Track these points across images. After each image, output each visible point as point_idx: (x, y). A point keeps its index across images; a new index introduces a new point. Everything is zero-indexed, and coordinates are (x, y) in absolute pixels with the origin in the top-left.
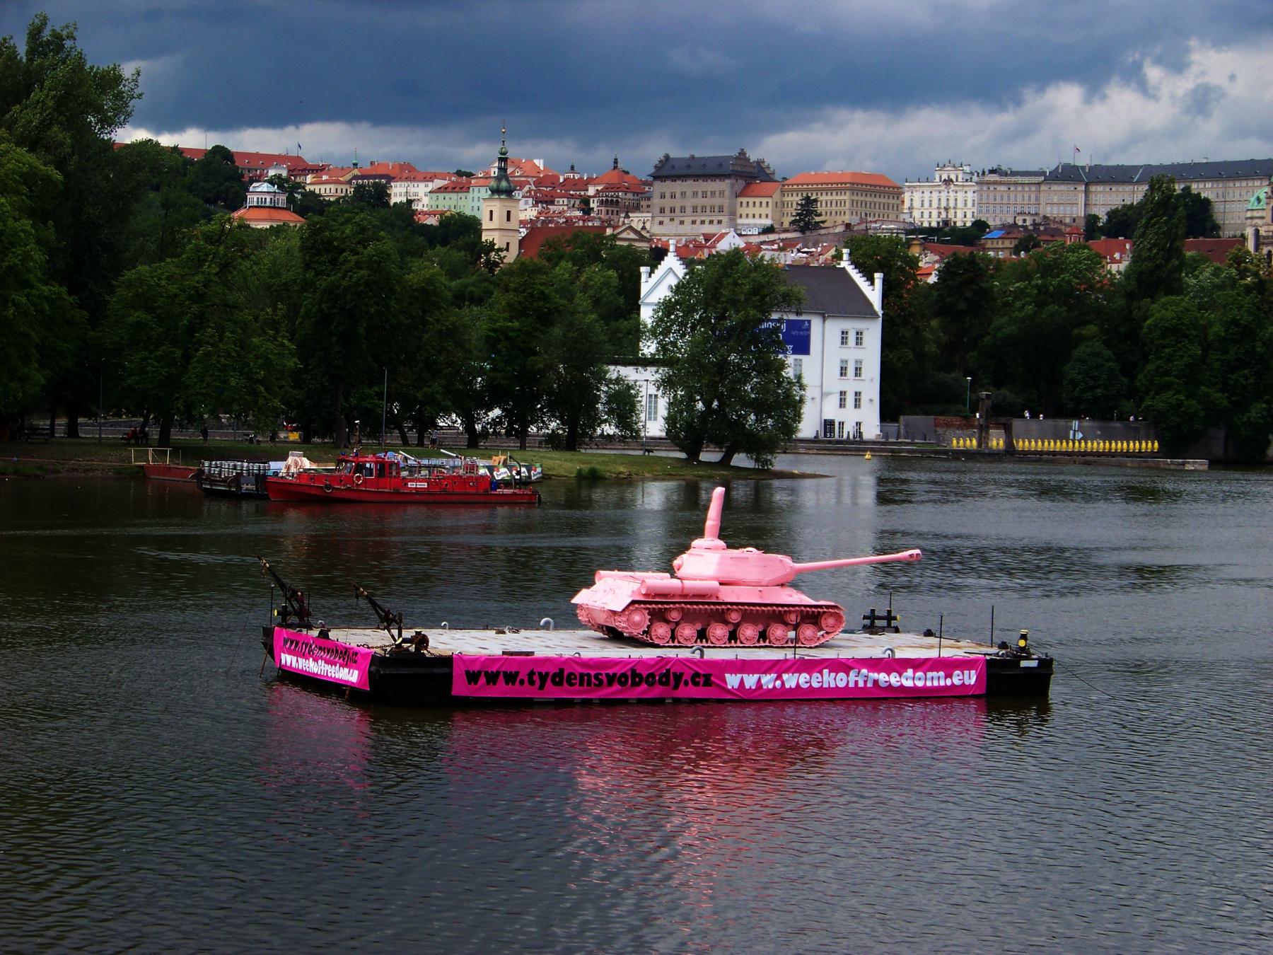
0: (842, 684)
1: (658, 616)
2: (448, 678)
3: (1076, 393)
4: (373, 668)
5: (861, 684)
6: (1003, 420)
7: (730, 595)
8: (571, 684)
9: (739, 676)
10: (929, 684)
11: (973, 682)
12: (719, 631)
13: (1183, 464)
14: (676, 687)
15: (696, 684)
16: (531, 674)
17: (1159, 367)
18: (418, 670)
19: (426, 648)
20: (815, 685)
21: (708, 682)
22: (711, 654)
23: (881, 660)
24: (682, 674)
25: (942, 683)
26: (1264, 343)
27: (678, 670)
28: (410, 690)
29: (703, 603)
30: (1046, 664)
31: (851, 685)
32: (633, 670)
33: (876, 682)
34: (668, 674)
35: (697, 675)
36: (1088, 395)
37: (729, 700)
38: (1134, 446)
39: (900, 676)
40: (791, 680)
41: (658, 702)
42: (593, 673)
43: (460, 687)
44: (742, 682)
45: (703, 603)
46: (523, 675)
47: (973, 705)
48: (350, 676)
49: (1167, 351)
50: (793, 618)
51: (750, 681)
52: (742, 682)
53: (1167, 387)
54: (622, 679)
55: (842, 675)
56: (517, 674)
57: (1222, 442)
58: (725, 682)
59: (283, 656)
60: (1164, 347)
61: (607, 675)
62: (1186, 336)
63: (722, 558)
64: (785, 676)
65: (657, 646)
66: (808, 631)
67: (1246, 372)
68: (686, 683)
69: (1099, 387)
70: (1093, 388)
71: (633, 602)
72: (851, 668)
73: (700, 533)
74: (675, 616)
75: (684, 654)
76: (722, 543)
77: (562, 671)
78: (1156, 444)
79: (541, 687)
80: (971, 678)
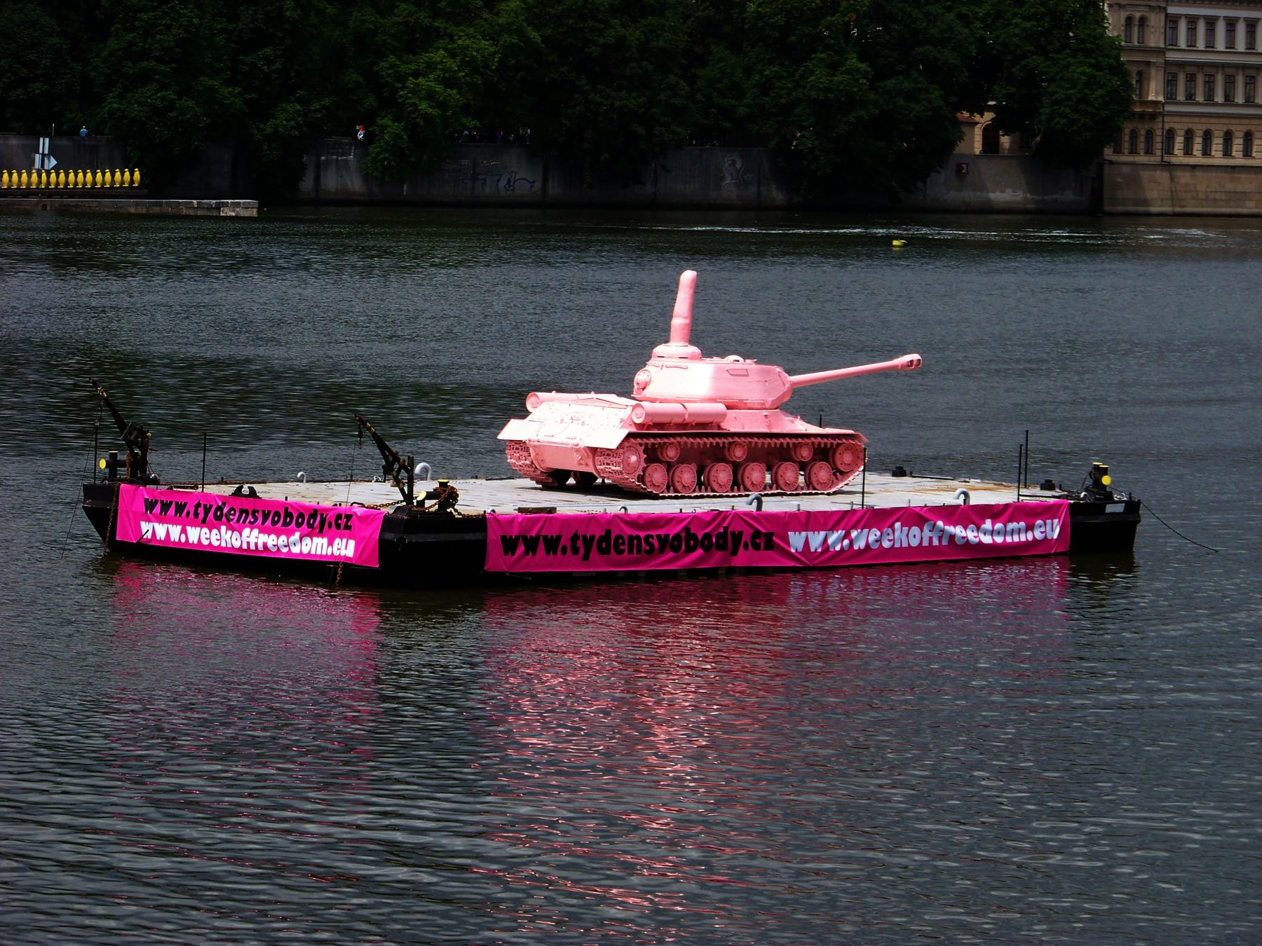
0: (914, 543)
1: (652, 456)
2: (481, 546)
4: (389, 536)
7: (736, 423)
8: (620, 552)
9: (804, 534)
10: (1009, 539)
12: (789, 473)
13: (218, 208)
14: (734, 553)
15: (756, 547)
16: (575, 537)
18: (442, 537)
19: (453, 506)
21: (770, 545)
22: (773, 505)
23: (1007, 506)
24: (741, 533)
25: (1023, 538)
28: (430, 565)
29: (700, 436)
30: (1133, 507)
32: (687, 529)
33: (952, 537)
34: (723, 534)
35: (757, 534)
37: (794, 570)
38: (103, 178)
39: (978, 529)
40: (862, 538)
41: (712, 573)
43: (497, 561)
44: (807, 543)
45: (700, 436)
46: (565, 541)
48: (345, 548)
49: (144, 17)
50: (805, 453)
51: (816, 540)
52: (807, 543)
55: (915, 530)
56: (559, 537)
58: (788, 543)
59: (145, 526)
61: (659, 537)
63: (718, 370)
65: (656, 497)
66: (822, 472)
67: (268, 50)
68: (564, 551)
71: (630, 435)
74: (671, 453)
76: (694, 350)
77: (608, 532)
78: (137, 175)
79: (586, 558)
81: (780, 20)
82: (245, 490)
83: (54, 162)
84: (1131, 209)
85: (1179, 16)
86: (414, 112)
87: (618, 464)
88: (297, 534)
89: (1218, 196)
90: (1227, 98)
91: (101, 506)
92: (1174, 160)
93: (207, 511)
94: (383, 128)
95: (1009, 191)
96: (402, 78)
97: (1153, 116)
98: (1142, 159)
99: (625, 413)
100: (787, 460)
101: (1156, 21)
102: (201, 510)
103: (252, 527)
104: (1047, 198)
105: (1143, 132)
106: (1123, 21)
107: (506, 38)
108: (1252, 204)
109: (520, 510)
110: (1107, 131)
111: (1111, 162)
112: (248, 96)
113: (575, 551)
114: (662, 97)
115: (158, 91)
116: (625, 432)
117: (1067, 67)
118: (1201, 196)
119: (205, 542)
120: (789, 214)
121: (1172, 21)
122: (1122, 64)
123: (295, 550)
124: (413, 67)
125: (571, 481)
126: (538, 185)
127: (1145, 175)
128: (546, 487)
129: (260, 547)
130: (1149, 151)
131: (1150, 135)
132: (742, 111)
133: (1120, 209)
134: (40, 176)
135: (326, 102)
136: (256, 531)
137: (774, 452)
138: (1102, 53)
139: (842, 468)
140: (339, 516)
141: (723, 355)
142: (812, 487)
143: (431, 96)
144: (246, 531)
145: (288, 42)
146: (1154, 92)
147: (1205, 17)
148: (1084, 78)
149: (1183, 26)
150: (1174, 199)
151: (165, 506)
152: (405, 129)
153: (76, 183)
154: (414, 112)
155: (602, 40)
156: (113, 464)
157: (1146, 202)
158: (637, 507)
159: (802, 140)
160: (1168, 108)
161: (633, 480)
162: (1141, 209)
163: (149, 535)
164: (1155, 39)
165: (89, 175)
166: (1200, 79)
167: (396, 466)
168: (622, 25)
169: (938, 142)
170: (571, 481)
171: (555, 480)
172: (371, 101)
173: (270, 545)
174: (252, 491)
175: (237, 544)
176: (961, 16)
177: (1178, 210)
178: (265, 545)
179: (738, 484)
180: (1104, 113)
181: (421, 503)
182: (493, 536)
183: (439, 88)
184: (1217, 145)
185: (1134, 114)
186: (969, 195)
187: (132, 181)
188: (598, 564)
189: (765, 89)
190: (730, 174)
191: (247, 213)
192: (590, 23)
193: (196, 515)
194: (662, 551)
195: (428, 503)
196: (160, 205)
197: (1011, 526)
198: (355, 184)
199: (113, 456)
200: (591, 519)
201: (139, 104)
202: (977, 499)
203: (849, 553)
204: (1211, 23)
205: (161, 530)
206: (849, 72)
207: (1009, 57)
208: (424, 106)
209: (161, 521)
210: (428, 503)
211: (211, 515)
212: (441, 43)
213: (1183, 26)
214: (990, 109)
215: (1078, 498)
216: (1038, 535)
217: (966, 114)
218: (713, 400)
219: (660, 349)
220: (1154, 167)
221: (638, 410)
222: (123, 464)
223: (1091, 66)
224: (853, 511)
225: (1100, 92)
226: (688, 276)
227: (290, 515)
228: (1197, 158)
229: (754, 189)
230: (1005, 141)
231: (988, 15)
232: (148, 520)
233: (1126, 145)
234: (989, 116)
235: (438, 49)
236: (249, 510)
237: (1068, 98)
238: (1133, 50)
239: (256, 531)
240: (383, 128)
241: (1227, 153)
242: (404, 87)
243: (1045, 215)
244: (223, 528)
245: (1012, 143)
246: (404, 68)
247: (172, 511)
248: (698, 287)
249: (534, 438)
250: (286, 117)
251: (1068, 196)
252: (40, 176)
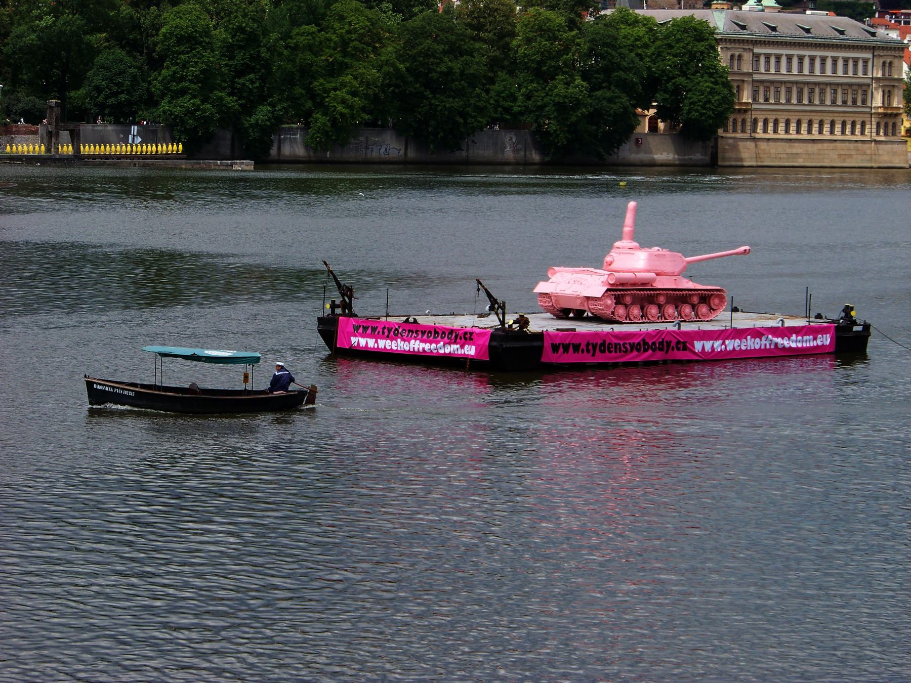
0: (757, 347)
1: (619, 300)
2: (541, 348)
3: (100, 99)
4: (494, 344)
5: (768, 347)
6: (71, 127)
7: (663, 283)
8: (610, 352)
11: (828, 343)
12: (653, 310)
13: (232, 165)
15: (678, 349)
16: (588, 344)
17: (175, 72)
20: (743, 348)
21: (685, 348)
22: (685, 327)
23: (803, 327)
26: (268, 49)
27: (576, 342)
28: (513, 359)
31: (763, 347)
32: (643, 340)
33: (776, 344)
34: (662, 342)
35: (679, 342)
36: (112, 101)
37: (697, 362)
38: (163, 148)
40: (731, 344)
42: (621, 343)
43: (548, 357)
44: (703, 347)
46: (583, 346)
47: (827, 362)
48: (470, 350)
49: (183, 57)
51: (708, 345)
52: (703, 347)
53: (183, 92)
54: (634, 347)
57: (228, 143)
59: (354, 340)
60: (180, 53)
62: (200, 43)
63: (650, 255)
64: (727, 342)
65: (621, 323)
66: (704, 309)
67: (252, 76)
68: (673, 349)
69: (122, 92)
70: (116, 94)
71: (608, 290)
72: (763, 335)
73: (620, 238)
74: (628, 300)
75: (670, 327)
76: (635, 244)
77: (604, 341)
78: (181, 147)
79: (594, 355)
80: (826, 340)
81: (538, 57)
82: (411, 320)
83: (140, 140)
84: (733, 163)
85: (760, 54)
86: (334, 111)
87: (601, 305)
88: (442, 343)
89: (782, 156)
90: (810, 101)
91: (328, 329)
92: (757, 136)
93: (389, 332)
94: (316, 120)
95: (665, 154)
96: (327, 91)
97: (746, 111)
98: (739, 135)
99: (604, 278)
100: (651, 303)
101: (747, 56)
102: (386, 331)
103: (416, 339)
104: (686, 157)
105: (740, 120)
106: (729, 57)
107: (386, 69)
108: (801, 160)
109: (558, 330)
110: (720, 120)
111: (722, 137)
112: (240, 102)
113: (588, 351)
114: (472, 101)
115: (191, 99)
116: (605, 288)
117: (698, 83)
118: (773, 156)
119: (388, 348)
120: (544, 168)
121: (757, 56)
122: (729, 82)
123: (442, 351)
124: (333, 84)
125: (571, 315)
126: (402, 152)
127: (741, 144)
128: (559, 318)
129: (421, 350)
130: (743, 131)
131: (744, 122)
132: (516, 109)
133: (727, 163)
134: (132, 148)
135: (285, 105)
136: (418, 342)
137: (679, 298)
138: (718, 77)
139: (714, 307)
140: (466, 333)
141: (650, 247)
142: (699, 318)
143: (343, 101)
144: (413, 341)
145: (263, 71)
146: (746, 97)
147: (775, 55)
148: (708, 90)
149: (762, 60)
150: (757, 157)
151: (365, 328)
152: (329, 120)
153: (142, 151)
154: (334, 111)
155: (439, 70)
156: (333, 306)
157: (741, 160)
158: (617, 328)
159: (550, 125)
160: (754, 106)
161: (609, 312)
162: (739, 164)
163: (356, 344)
164: (747, 68)
165: (175, 146)
166: (772, 89)
167: (496, 306)
168: (450, 61)
169: (624, 127)
170: (571, 315)
171: (563, 314)
172: (309, 104)
173: (426, 349)
174: (415, 320)
175: (407, 349)
176: (637, 55)
177: (759, 164)
178: (423, 349)
179: (663, 316)
180: (720, 109)
181: (510, 326)
182: (547, 344)
183: (348, 97)
184: (782, 127)
185: (735, 110)
186: (642, 156)
187: (178, 150)
188: (600, 358)
189: (528, 97)
190: (509, 146)
191: (247, 168)
192: (432, 60)
193: (383, 333)
194: (632, 351)
195: (514, 326)
196: (199, 163)
197: (806, 338)
198: (300, 151)
199: (333, 302)
200: (596, 334)
201: (180, 107)
202: (789, 323)
203: (725, 352)
204: (778, 58)
205: (363, 342)
206: (577, 86)
207: (665, 78)
208: (340, 108)
209: (363, 337)
210: (514, 326)
211: (391, 333)
212: (348, 71)
213: (762, 60)
214: (653, 107)
215: (838, 323)
216: (820, 343)
217: (640, 110)
218: (649, 271)
219: (617, 244)
220: (747, 139)
221: (612, 277)
222: (338, 306)
223: (712, 82)
224: (726, 330)
225: (717, 98)
226: (632, 204)
227: (438, 333)
228: (770, 135)
229: (522, 153)
230: (661, 125)
231: (653, 54)
232: (356, 336)
233: (730, 128)
234: (652, 112)
235: (347, 74)
236: (412, 329)
237: (700, 101)
238: (734, 73)
239: (418, 342)
240: (316, 120)
241: (787, 131)
242: (328, 96)
243: (684, 168)
244: (399, 340)
245: (665, 127)
246: (328, 86)
247: (369, 331)
248: (636, 210)
249: (554, 291)
250: (262, 113)
251: (698, 156)
252: (132, 148)
